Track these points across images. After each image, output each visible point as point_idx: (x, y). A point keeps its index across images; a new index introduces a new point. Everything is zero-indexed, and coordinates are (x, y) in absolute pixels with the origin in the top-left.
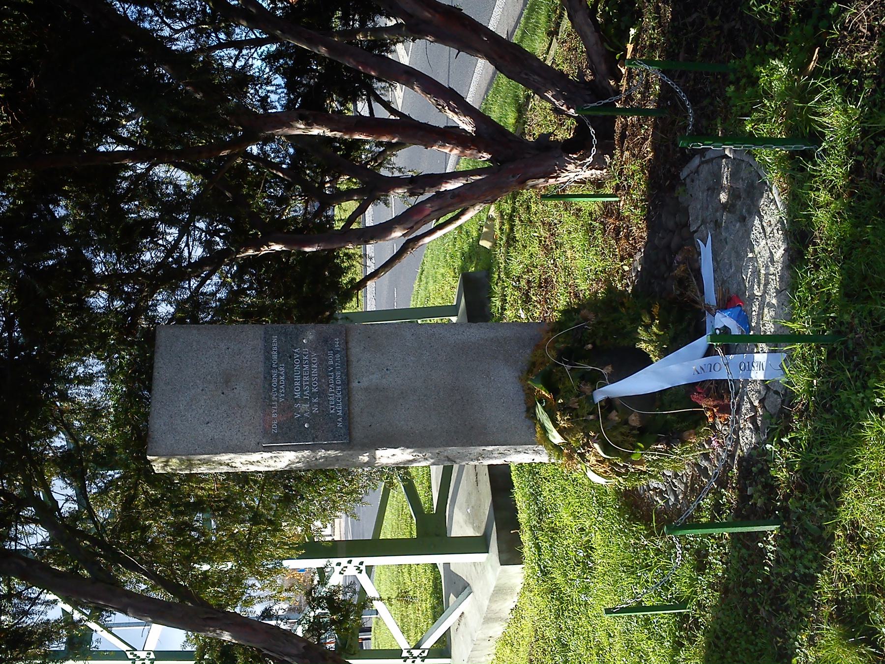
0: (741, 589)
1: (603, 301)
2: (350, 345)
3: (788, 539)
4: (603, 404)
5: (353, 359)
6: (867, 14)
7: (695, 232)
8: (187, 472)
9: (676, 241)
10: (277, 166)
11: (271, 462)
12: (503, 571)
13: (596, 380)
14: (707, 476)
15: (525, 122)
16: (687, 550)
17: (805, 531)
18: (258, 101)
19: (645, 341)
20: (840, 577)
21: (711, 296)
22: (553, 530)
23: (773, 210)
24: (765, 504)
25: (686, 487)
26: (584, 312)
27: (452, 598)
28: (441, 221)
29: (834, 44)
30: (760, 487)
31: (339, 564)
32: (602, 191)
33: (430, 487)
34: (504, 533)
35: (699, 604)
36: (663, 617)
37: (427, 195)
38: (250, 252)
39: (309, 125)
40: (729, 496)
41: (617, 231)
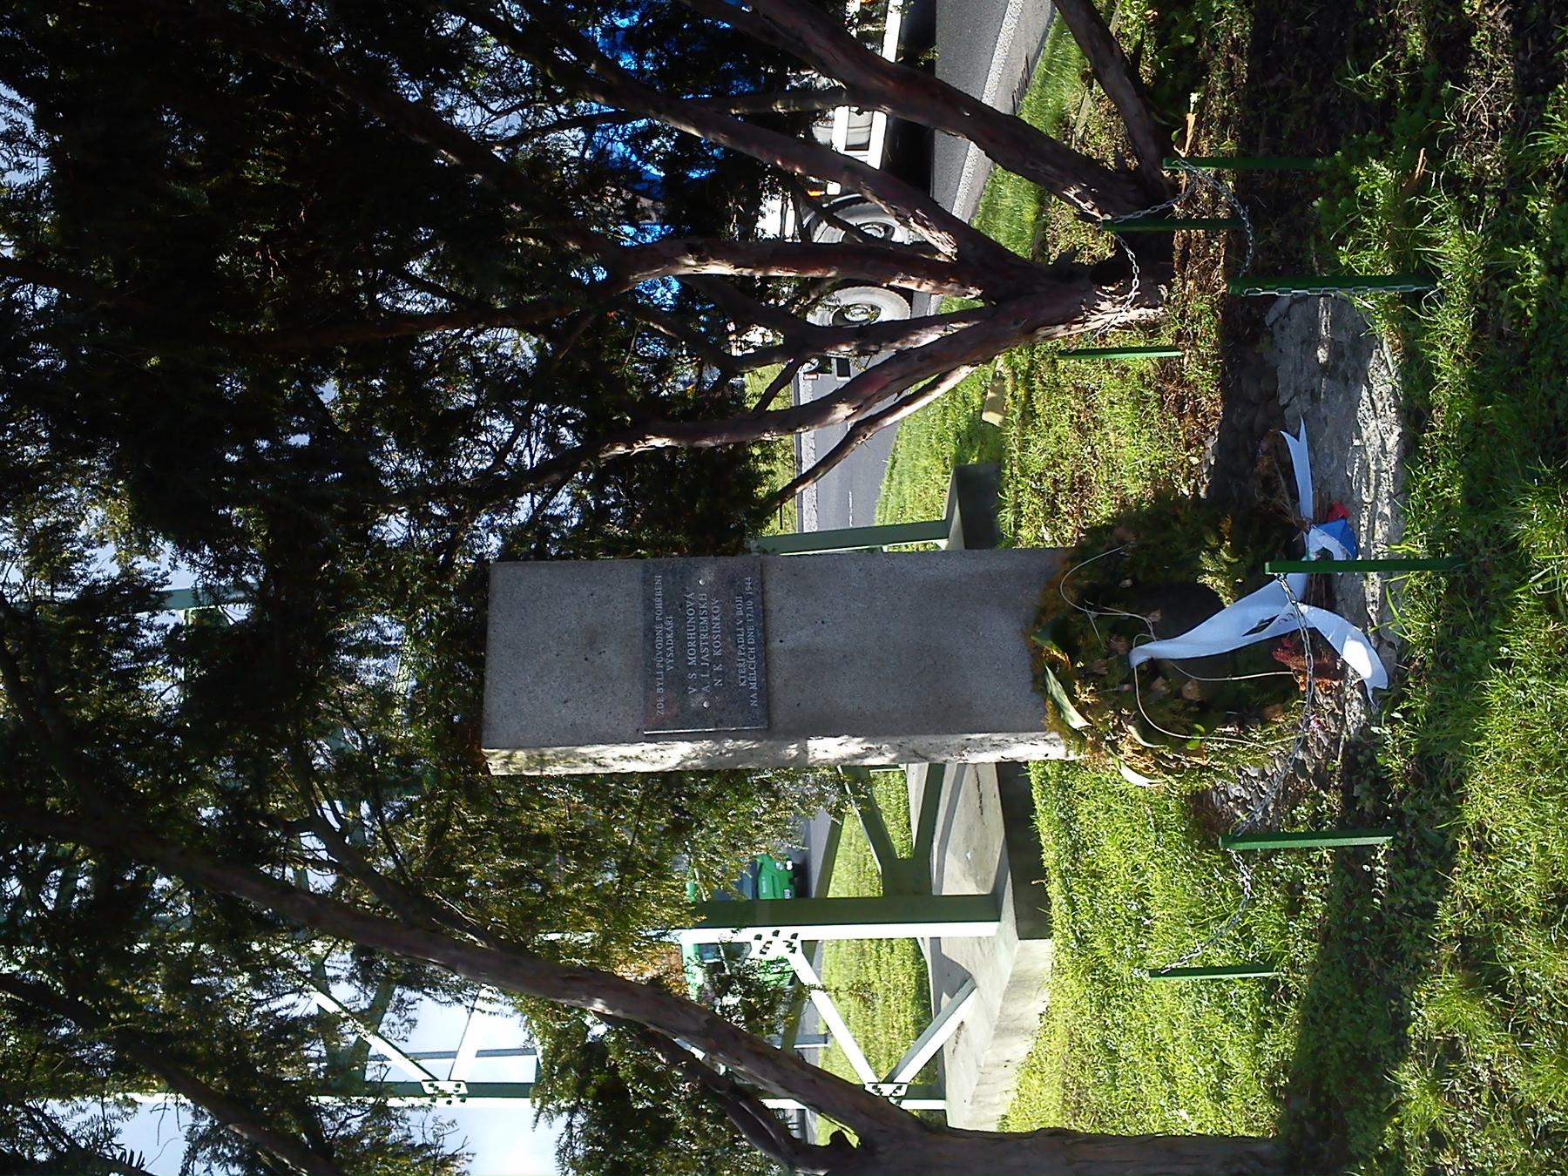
0: (1345, 933)
1: (1149, 515)
3: (1403, 856)
4: (1145, 667)
7: (1286, 406)
8: (537, 773)
9: (1260, 418)
11: (656, 756)
12: (1023, 949)
13: (1134, 633)
14: (1305, 774)
15: (1046, 225)
16: (1275, 884)
17: (1423, 842)
18: (622, 208)
19: (1211, 574)
20: (1464, 904)
21: (1307, 504)
22: (1095, 875)
24: (1374, 808)
26: (1119, 531)
27: (945, 998)
29: (1450, 140)
30: (1367, 783)
31: (759, 937)
32: (1156, 342)
33: (909, 825)
34: (1023, 890)
36: (1242, 988)
38: (621, 450)
39: (702, 260)
40: (1332, 799)
41: (1180, 403)
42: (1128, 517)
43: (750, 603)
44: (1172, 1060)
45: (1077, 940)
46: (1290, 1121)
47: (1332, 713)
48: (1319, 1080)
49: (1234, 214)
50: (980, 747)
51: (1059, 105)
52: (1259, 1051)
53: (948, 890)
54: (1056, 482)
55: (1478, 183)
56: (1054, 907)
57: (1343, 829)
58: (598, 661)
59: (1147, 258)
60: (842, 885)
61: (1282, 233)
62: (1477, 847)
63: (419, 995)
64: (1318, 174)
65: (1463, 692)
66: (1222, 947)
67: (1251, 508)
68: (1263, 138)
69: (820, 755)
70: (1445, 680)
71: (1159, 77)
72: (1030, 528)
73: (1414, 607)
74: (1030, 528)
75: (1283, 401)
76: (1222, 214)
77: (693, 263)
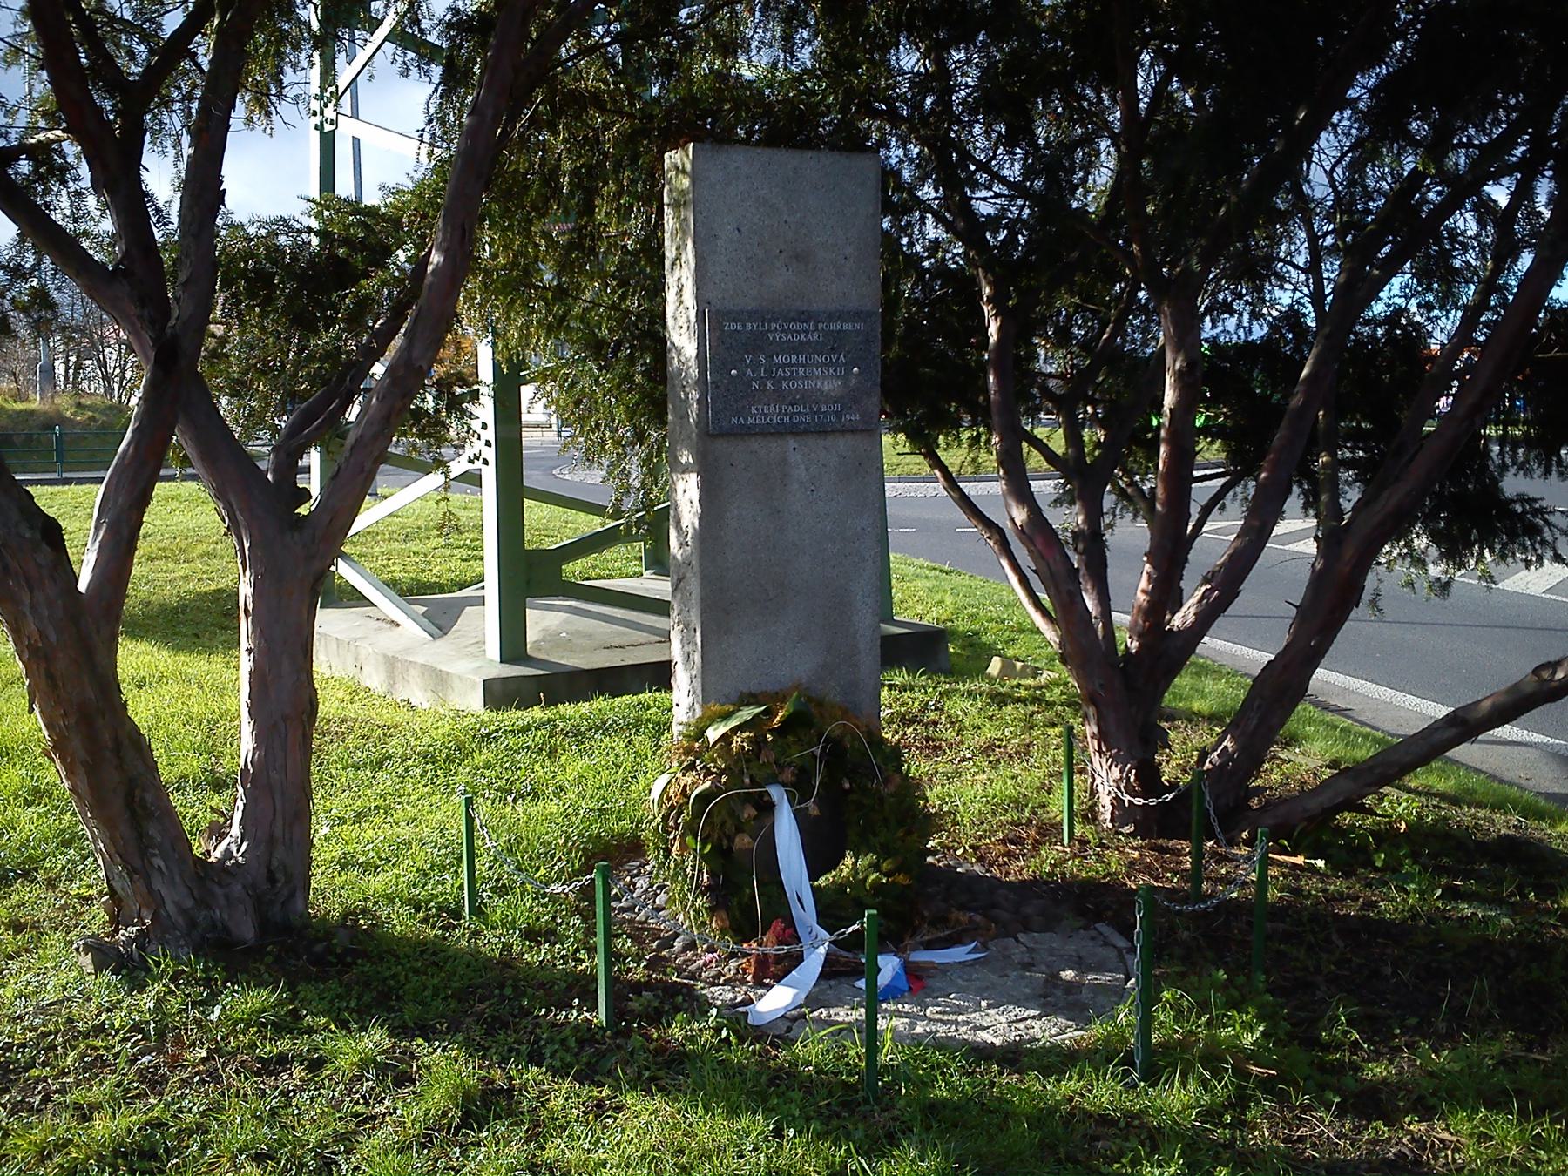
1: (913, 806)
2: (849, 437)
3: (587, 1036)
5: (829, 441)
6: (1321, 1134)
7: (1017, 940)
8: (666, 200)
10: (1119, 329)
11: (682, 321)
12: (474, 684)
13: (799, 790)
14: (661, 948)
15: (1190, 721)
20: (544, 1092)
23: (1047, 1030)
25: (640, 922)
26: (897, 778)
28: (1035, 580)
29: (1282, 1099)
30: (656, 1004)
31: (484, 426)
34: (529, 685)
35: (477, 933)
36: (452, 885)
37: (1076, 560)
38: (987, 291)
40: (639, 973)
41: (1018, 841)
42: (911, 789)
43: (834, 419)
44: (377, 820)
45: (488, 735)
46: (325, 930)
47: (720, 974)
48: (365, 955)
49: (1205, 898)
50: (687, 641)
51: (1307, 738)
52: (392, 901)
53: (531, 614)
54: (935, 724)
55: (1240, 1124)
56: (519, 713)
57: (612, 981)
58: (778, 264)
59: (1160, 816)
60: (535, 513)
61: (1194, 941)
62: (600, 1105)
63: (436, 80)
64: (1248, 977)
65: (748, 1093)
66: (490, 868)
67: (920, 905)
68: (1281, 926)
69: (680, 486)
70: (761, 1079)
71: (1341, 832)
72: (898, 695)
73: (828, 1052)
74: (898, 695)
75: (1021, 936)
76: (1205, 885)
77: (1178, 366)
